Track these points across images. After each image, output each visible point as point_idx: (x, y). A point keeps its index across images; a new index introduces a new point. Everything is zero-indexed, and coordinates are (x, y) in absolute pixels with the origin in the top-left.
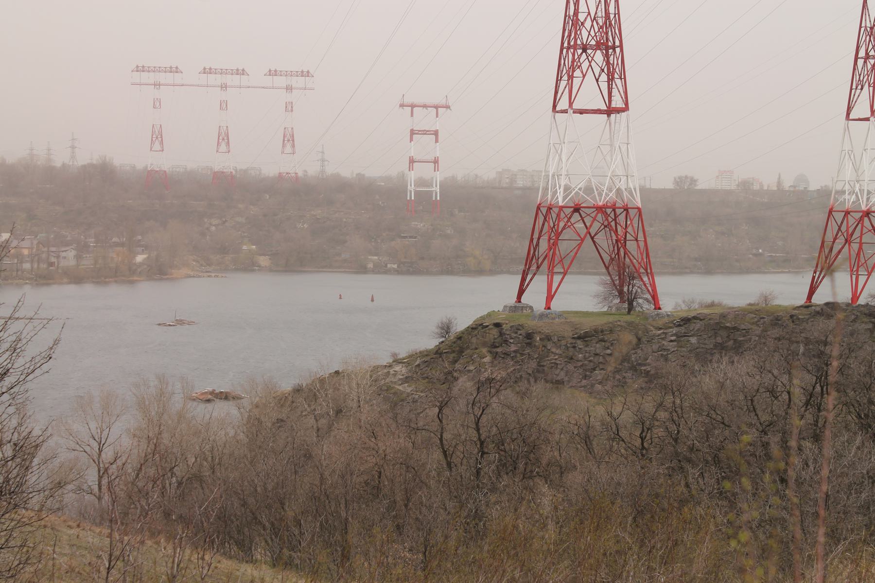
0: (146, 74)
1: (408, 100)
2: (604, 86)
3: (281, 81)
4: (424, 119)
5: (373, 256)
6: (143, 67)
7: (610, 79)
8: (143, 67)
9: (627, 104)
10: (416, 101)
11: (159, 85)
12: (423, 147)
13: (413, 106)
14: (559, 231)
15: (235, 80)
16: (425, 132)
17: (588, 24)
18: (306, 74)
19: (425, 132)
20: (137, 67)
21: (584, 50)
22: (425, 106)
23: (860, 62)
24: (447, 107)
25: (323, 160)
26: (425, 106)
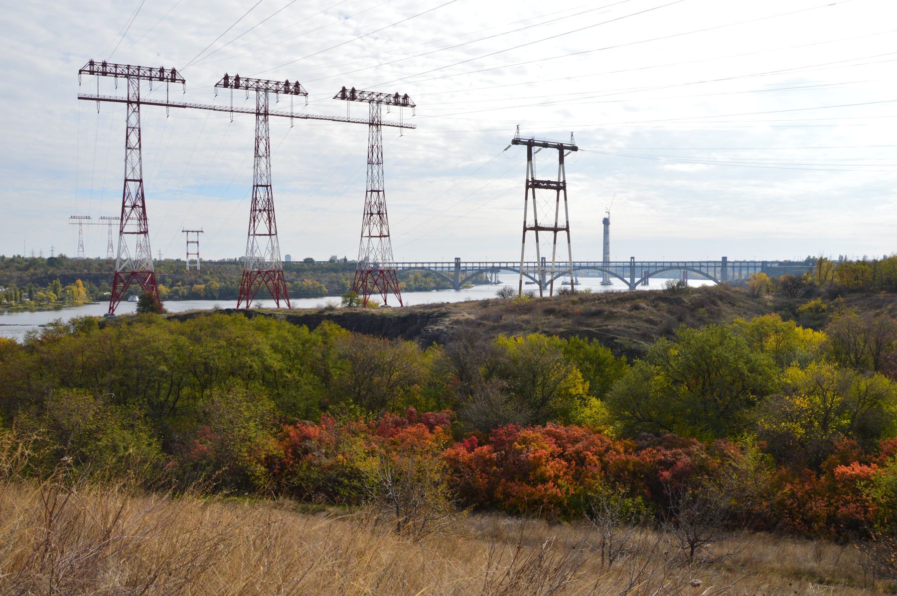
0: (110, 79)
1: (186, 229)
2: (268, 225)
3: (361, 110)
4: (193, 237)
5: (585, 330)
6: (104, 64)
7: (270, 222)
8: (104, 64)
9: (276, 232)
10: (189, 230)
11: (138, 103)
12: (193, 248)
13: (188, 232)
14: (625, 279)
15: (86, 221)
16: (193, 242)
17: (261, 202)
18: (402, 101)
19: (193, 242)
20: (92, 63)
21: (264, 209)
22: (193, 232)
23: (366, 215)
24: (202, 232)
25: (160, 254)
26: (193, 232)
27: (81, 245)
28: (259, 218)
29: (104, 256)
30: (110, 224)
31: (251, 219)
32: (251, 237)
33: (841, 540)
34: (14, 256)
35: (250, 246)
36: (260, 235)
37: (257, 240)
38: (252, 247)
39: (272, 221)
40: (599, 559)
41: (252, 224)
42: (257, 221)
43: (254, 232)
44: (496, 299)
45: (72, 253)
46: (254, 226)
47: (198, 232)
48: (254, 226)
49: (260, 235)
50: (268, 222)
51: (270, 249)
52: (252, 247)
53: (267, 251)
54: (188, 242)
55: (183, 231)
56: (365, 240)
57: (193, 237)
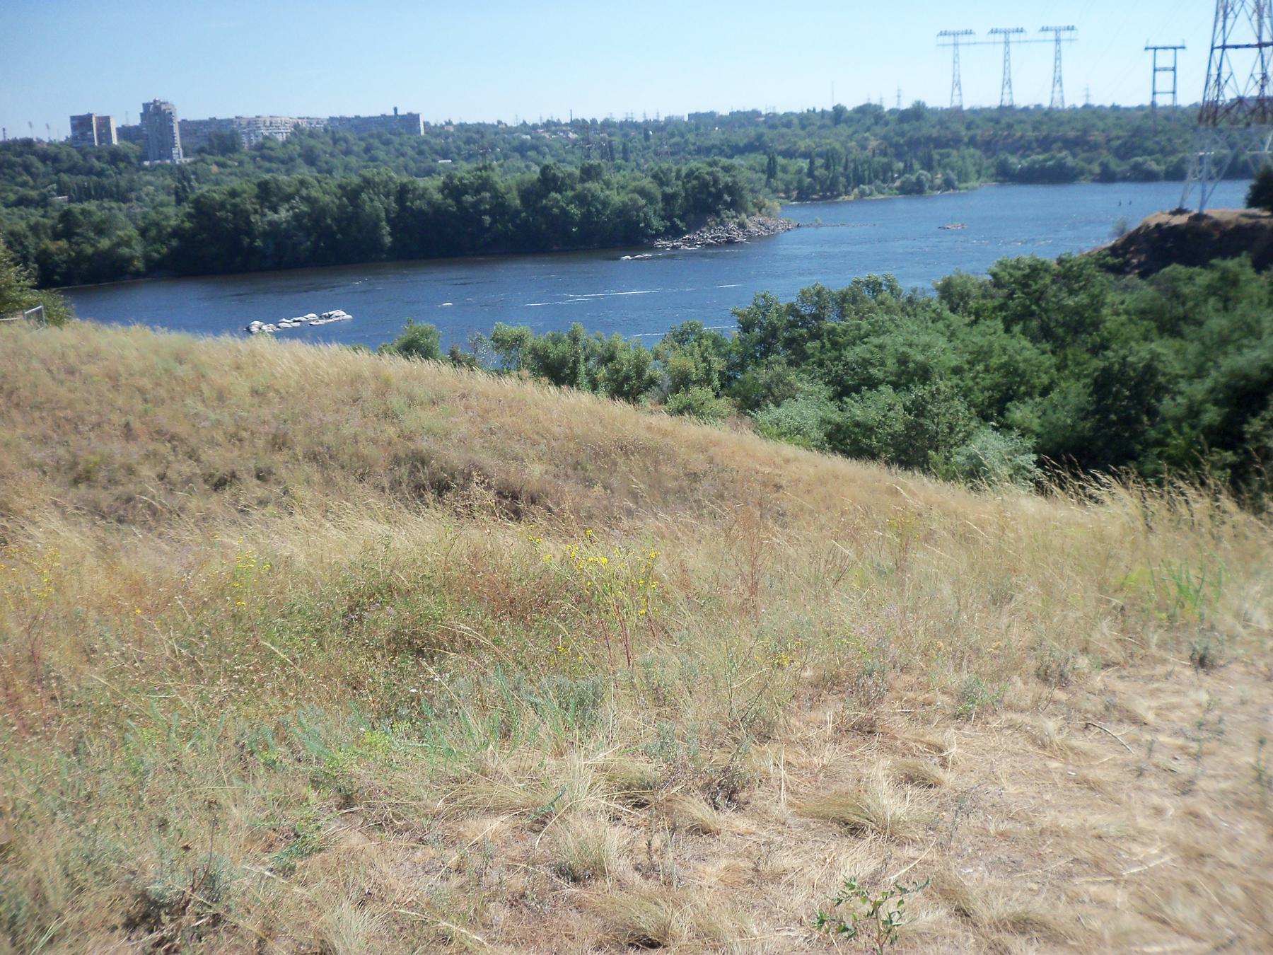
1: (1151, 44)
4: (1165, 59)
7: (1261, 17)
13: (1155, 49)
22: (1165, 48)
26: (1165, 48)
27: (957, 84)
28: (1237, 8)
29: (946, 105)
30: (956, 45)
31: (1217, 13)
32: (1218, 52)
33: (497, 815)
34: (156, 114)
35: (1214, 72)
36: (1237, 47)
37: (1230, 56)
38: (1219, 75)
39: (1265, 15)
40: (1208, 859)
41: (1220, 25)
42: (1231, 15)
43: (1224, 41)
44: (1253, 187)
45: (938, 98)
46: (1224, 27)
47: (1175, 48)
48: (1224, 27)
49: (1237, 47)
50: (1255, 17)
51: (1258, 77)
52: (1219, 75)
53: (1252, 83)
54: (1155, 70)
55: (1146, 49)
56: (1218, 52)
57: (1165, 59)
